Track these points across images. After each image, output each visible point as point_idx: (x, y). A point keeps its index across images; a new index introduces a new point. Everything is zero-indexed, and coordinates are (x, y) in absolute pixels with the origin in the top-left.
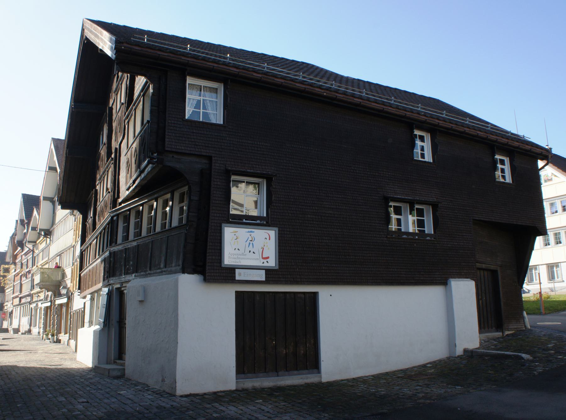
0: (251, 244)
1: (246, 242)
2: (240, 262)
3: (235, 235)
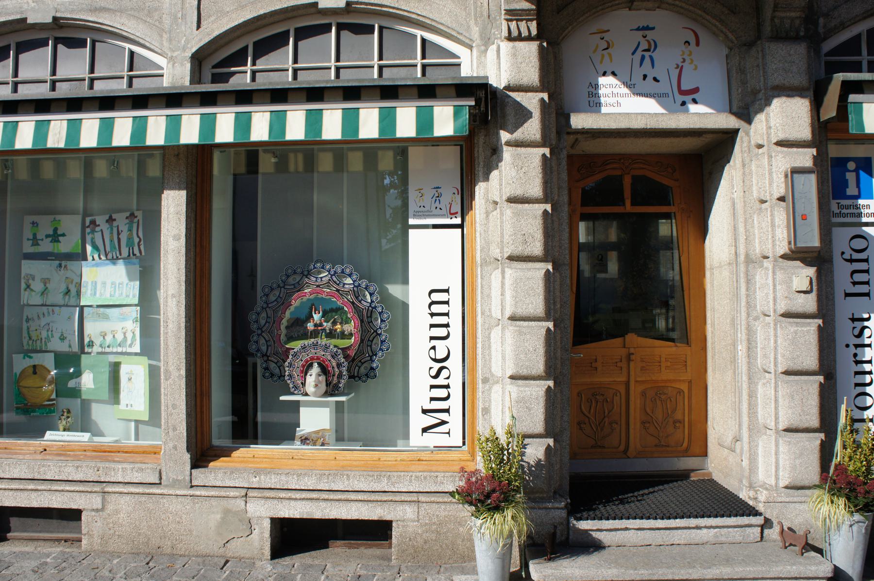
0: (438, 200)
1: (633, 54)
2: (619, 104)
3: (603, 39)
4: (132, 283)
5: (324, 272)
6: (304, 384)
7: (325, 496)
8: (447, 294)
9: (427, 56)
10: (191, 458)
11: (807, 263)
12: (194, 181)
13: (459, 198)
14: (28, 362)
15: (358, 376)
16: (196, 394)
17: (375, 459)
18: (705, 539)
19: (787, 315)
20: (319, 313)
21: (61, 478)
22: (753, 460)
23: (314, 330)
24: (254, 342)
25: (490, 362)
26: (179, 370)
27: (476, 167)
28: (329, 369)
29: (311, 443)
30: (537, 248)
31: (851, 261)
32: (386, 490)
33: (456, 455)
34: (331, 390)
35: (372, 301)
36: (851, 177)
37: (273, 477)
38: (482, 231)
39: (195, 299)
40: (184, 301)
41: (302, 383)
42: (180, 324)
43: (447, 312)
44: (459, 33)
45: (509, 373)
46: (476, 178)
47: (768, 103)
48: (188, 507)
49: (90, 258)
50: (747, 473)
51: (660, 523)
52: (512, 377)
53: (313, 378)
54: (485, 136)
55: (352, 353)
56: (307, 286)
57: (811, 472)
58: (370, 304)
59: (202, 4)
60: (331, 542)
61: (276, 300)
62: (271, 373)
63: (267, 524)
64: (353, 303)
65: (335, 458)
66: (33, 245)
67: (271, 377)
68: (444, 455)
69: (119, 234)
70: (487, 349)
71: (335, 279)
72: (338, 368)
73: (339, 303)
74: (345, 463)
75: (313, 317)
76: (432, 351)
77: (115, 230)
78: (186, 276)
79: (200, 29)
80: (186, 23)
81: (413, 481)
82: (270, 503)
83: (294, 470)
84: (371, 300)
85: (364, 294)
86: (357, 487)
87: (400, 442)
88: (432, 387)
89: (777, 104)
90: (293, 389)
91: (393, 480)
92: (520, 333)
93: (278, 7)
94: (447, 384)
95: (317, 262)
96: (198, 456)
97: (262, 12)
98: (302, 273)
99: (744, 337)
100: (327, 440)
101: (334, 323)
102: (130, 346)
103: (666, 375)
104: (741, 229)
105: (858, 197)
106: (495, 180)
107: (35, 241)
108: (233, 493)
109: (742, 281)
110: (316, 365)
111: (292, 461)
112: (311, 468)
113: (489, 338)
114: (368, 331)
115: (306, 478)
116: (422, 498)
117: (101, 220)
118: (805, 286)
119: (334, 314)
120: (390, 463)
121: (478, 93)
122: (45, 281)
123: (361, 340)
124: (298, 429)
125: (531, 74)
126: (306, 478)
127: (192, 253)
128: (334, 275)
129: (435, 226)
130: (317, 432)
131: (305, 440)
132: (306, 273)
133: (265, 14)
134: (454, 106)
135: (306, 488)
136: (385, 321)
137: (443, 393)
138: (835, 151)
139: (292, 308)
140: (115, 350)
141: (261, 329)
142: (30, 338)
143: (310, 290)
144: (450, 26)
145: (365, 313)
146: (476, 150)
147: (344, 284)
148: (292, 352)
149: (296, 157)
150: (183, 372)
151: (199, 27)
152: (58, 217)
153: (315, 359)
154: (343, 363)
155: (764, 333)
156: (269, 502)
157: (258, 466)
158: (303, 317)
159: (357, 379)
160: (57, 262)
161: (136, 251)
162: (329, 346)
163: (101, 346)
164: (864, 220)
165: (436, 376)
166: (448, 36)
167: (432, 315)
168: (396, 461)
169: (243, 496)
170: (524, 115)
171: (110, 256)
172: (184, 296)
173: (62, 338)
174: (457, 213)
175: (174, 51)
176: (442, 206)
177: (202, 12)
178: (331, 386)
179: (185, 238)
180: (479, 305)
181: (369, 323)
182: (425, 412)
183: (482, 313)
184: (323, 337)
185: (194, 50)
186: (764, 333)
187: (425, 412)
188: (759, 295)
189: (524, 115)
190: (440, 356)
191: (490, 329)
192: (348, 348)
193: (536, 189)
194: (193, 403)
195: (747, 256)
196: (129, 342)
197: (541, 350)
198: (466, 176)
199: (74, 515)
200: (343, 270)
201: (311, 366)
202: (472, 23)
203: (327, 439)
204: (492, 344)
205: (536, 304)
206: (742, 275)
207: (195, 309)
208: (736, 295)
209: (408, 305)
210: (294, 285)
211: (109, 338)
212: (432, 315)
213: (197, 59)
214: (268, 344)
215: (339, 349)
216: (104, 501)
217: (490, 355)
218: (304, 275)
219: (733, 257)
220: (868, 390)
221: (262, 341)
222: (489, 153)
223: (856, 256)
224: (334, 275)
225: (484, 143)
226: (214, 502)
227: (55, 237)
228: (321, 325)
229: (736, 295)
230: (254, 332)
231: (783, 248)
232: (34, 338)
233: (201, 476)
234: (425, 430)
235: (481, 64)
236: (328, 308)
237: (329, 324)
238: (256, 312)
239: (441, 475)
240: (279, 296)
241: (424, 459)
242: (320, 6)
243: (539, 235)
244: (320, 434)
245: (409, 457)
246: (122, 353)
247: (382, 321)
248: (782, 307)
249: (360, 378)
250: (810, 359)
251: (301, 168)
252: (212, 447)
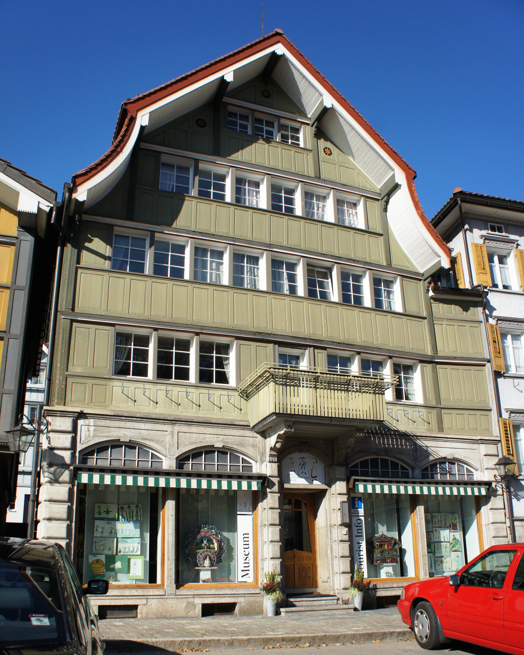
4: (137, 530)
7: (217, 596)
11: (346, 527)
14: (95, 558)
18: (323, 604)
19: (341, 541)
21: (131, 595)
22: (333, 582)
26: (172, 557)
30: (277, 522)
31: (357, 526)
34: (212, 565)
36: (356, 502)
45: (270, 557)
47: (335, 482)
49: (121, 520)
50: (332, 587)
51: (312, 599)
52: (271, 558)
53: (207, 563)
57: (348, 583)
60: (214, 614)
63: (200, 606)
66: (99, 515)
69: (132, 512)
77: (131, 511)
82: (201, 599)
88: (244, 563)
89: (338, 483)
92: (274, 546)
97: (198, 446)
99: (330, 548)
102: (136, 552)
103: (305, 562)
104: (328, 517)
105: (358, 508)
107: (100, 513)
108: (190, 596)
109: (329, 532)
116: (246, 595)
117: (125, 507)
118: (346, 533)
122: (103, 528)
125: (276, 473)
130: (208, 579)
131: (204, 581)
137: (247, 565)
138: (352, 495)
140: (129, 554)
142: (96, 549)
150: (174, 558)
152: (108, 505)
155: (335, 546)
156: (201, 598)
160: (107, 521)
161: (139, 519)
163: (124, 552)
164: (360, 515)
165: (246, 560)
167: (244, 541)
170: (273, 484)
171: (129, 520)
173: (109, 549)
182: (242, 571)
185: (177, 456)
186: (335, 546)
187: (242, 571)
188: (333, 536)
189: (273, 484)
190: (246, 554)
193: (277, 505)
195: (330, 525)
196: (135, 551)
197: (279, 551)
199: (135, 607)
201: (206, 558)
205: (277, 537)
206: (329, 530)
208: (327, 536)
211: (127, 550)
212: (244, 541)
216: (147, 601)
219: (326, 525)
220: (362, 563)
223: (358, 525)
226: (184, 600)
227: (108, 512)
229: (327, 536)
231: (340, 523)
232: (98, 549)
233: (179, 592)
234: (242, 576)
235: (260, 468)
243: (278, 518)
246: (132, 555)
248: (340, 539)
250: (347, 553)
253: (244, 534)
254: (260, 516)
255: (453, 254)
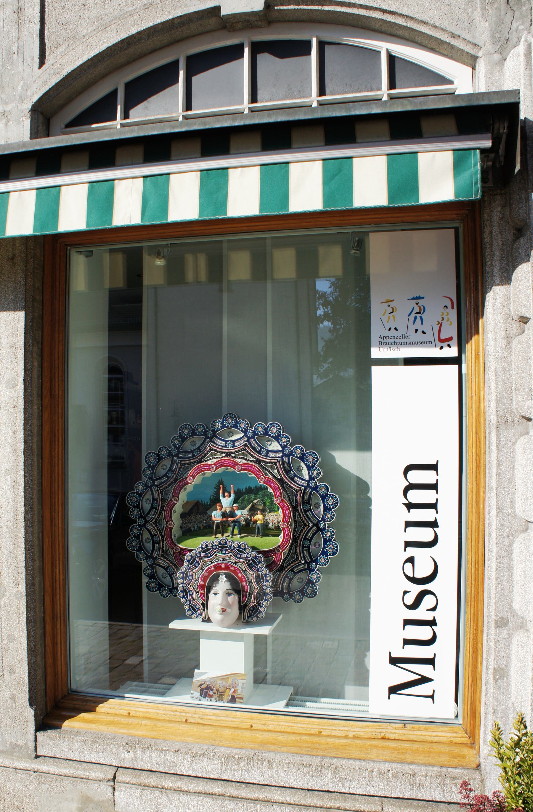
5: (237, 433)
6: (205, 606)
7: (232, 791)
8: (434, 472)
9: (397, 83)
10: (36, 716)
12: (39, 297)
13: (453, 314)
15: (288, 593)
16: (44, 617)
17: (312, 732)
20: (230, 496)
23: (222, 522)
24: (135, 536)
25: (511, 591)
26: (17, 584)
27: (488, 258)
28: (244, 584)
29: (215, 696)
32: (330, 790)
33: (444, 734)
35: (311, 479)
37: (154, 754)
38: (500, 369)
39: (42, 476)
40: (23, 480)
41: (203, 604)
42: (17, 515)
43: (434, 502)
44: (453, 36)
46: (489, 280)
48: (31, 788)
54: (503, 207)
55: (279, 559)
56: (212, 454)
58: (308, 482)
59: (46, 28)
61: (165, 475)
62: (159, 583)
64: (281, 481)
65: (251, 726)
67: (159, 589)
68: (425, 733)
70: (505, 569)
71: (255, 445)
72: (258, 583)
73: (260, 482)
74: (267, 736)
75: (219, 501)
76: (409, 565)
78: (25, 442)
79: (44, 66)
80: (24, 60)
81: (375, 779)
83: (188, 743)
84: (310, 476)
85: (299, 467)
86: (284, 780)
87: (350, 689)
88: (407, 622)
90: (190, 612)
91: (342, 774)
93: (158, 21)
94: (432, 619)
95: (227, 417)
96: (49, 709)
98: (205, 434)
100: (239, 693)
101: (253, 511)
106: (524, 280)
110: (223, 578)
111: (185, 728)
112: (213, 742)
113: (510, 552)
114: (305, 525)
115: (205, 761)
119: (252, 496)
120: (337, 741)
121: (496, 126)
123: (293, 538)
124: (196, 671)
126: (205, 761)
127: (35, 407)
128: (253, 437)
129: (409, 362)
130: (225, 678)
132: (210, 434)
133: (138, 33)
134: (454, 150)
135: (205, 776)
136: (330, 509)
137: (425, 633)
139: (189, 488)
141: (144, 518)
143: (215, 460)
144: (438, 25)
145: (299, 496)
146: (487, 231)
147: (269, 451)
148: (188, 555)
149: (196, 260)
150: (22, 588)
151: (42, 62)
153: (222, 569)
154: (266, 575)
156: (148, 794)
157: (133, 732)
158: (206, 500)
159: (286, 597)
162: (245, 549)
166: (433, 45)
167: (410, 506)
168: (346, 737)
169: (109, 780)
172: (23, 473)
174: (450, 339)
175: (6, 103)
176: (426, 327)
177: (46, 41)
178: (247, 611)
179: (22, 385)
180: (494, 494)
181: (306, 511)
182: (394, 661)
183: (498, 508)
184: (236, 531)
185: (35, 99)
187: (394, 661)
190: (419, 575)
191: (512, 536)
192: (273, 551)
194: (39, 632)
198: (466, 278)
200: (266, 429)
201: (216, 579)
202: (477, 14)
203: (239, 691)
204: (514, 563)
207: (41, 491)
209: (371, 499)
210: (192, 452)
212: (410, 506)
213: (42, 113)
214: (155, 539)
215: (259, 552)
217: (510, 580)
218: (207, 437)
221: (146, 535)
222: (510, 236)
224: (253, 437)
225: (502, 219)
226: (68, 784)
228: (232, 514)
230: (135, 522)
234: (393, 690)
236: (243, 487)
237: (245, 512)
238: (137, 493)
239: (420, 770)
240: (170, 469)
241: (392, 736)
242: (224, 12)
244: (230, 681)
245: (367, 733)
247: (326, 509)
249: (291, 596)
251: (203, 276)
252: (72, 694)
253: (409, 468)
254: (492, 364)
255: (529, 87)
